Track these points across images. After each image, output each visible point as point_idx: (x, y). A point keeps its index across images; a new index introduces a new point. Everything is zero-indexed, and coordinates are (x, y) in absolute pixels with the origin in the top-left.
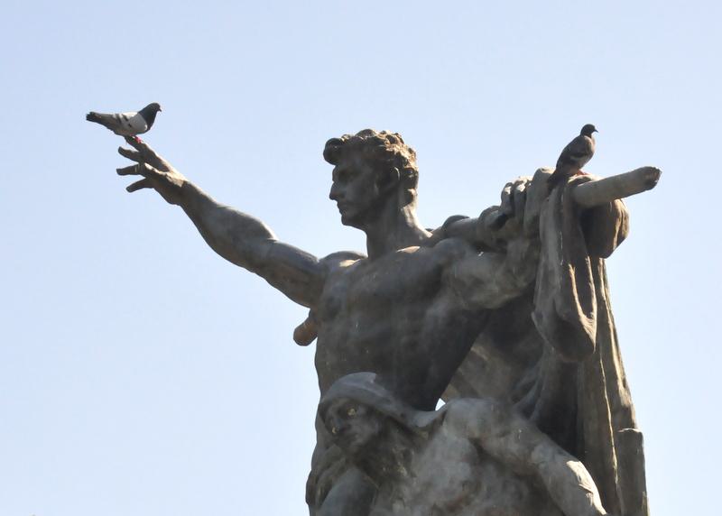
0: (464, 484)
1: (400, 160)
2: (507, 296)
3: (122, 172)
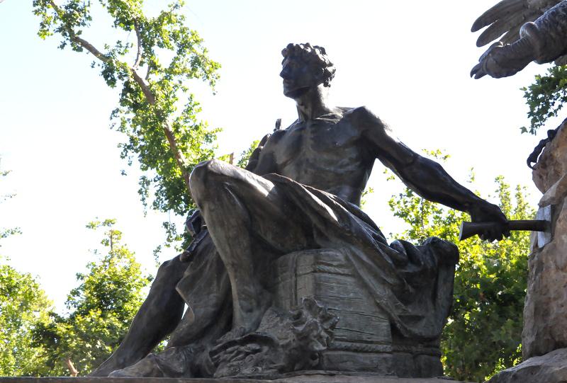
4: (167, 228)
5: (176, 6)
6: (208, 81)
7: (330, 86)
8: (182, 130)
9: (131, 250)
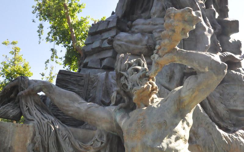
4: (53, 51)
8: (73, 6)
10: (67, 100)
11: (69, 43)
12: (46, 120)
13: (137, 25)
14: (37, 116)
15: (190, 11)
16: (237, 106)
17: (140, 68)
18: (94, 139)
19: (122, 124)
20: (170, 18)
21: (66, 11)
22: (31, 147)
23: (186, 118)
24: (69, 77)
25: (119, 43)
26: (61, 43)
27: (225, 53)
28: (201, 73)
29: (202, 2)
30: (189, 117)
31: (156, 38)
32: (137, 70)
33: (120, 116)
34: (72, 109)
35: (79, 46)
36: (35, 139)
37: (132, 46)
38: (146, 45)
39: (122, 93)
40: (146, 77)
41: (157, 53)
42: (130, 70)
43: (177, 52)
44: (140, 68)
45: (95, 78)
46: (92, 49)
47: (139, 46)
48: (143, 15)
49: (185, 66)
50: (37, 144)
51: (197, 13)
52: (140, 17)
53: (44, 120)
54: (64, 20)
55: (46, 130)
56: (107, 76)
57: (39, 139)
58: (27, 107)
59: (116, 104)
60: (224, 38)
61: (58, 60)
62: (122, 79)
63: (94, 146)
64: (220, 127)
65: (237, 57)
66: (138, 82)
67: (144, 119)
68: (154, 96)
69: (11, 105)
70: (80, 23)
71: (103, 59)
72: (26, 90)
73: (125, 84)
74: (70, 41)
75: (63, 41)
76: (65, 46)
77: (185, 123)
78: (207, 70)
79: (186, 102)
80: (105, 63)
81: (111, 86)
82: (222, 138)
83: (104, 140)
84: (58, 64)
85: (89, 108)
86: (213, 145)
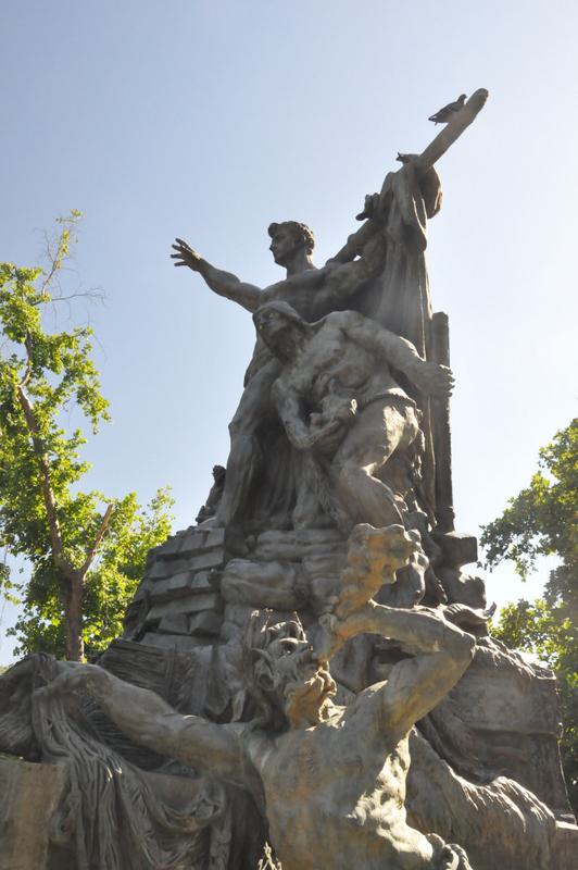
0: (335, 351)
1: (306, 233)
2: (360, 281)
3: (173, 256)
5: (83, 333)
6: (91, 417)
7: (79, 402)
9: (496, 569)
10: (139, 709)
11: (44, 551)
12: (96, 755)
13: (269, 542)
14: (76, 747)
15: (400, 532)
16: (486, 722)
17: (294, 641)
18: (197, 799)
19: (263, 764)
20: (360, 543)
21: (43, 478)
22: (57, 820)
23: (397, 750)
24: (133, 656)
25: (235, 581)
26: (22, 550)
27: (454, 605)
28: (420, 654)
29: (401, 500)
30: (403, 747)
31: (312, 573)
32: (290, 646)
33: (258, 746)
34: (151, 729)
35: (69, 559)
36: (68, 799)
37: (262, 590)
38: (292, 588)
39: (257, 694)
40: (311, 663)
41: (332, 613)
42: (275, 645)
43: (375, 610)
44: (294, 641)
45: (189, 658)
46: (169, 590)
47: (278, 590)
48: (272, 519)
49: (378, 635)
50: (71, 813)
51: (412, 535)
52: (269, 525)
53: (90, 755)
54: (38, 497)
55: (96, 777)
56: (215, 654)
57: (78, 801)
58: (49, 723)
59: (242, 720)
60: (449, 573)
61: (13, 592)
62: (260, 664)
63: (199, 816)
64: (458, 773)
65: (479, 613)
66: (295, 671)
67: (313, 752)
68: (328, 702)
69: (12, 719)
70: (75, 507)
71: (191, 615)
72: (51, 686)
73: (265, 676)
74: (47, 547)
75: (28, 546)
76: (33, 559)
77: (397, 762)
78: (436, 648)
79: (397, 716)
80: (197, 622)
81: (226, 678)
82: (465, 797)
83: (219, 802)
84: (11, 603)
85: (188, 727)
86: (447, 813)
